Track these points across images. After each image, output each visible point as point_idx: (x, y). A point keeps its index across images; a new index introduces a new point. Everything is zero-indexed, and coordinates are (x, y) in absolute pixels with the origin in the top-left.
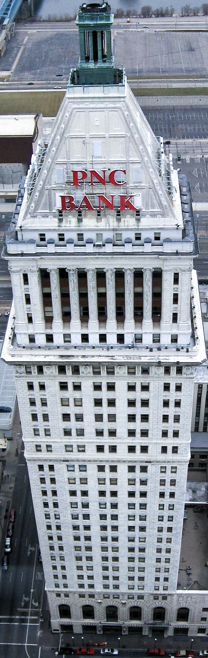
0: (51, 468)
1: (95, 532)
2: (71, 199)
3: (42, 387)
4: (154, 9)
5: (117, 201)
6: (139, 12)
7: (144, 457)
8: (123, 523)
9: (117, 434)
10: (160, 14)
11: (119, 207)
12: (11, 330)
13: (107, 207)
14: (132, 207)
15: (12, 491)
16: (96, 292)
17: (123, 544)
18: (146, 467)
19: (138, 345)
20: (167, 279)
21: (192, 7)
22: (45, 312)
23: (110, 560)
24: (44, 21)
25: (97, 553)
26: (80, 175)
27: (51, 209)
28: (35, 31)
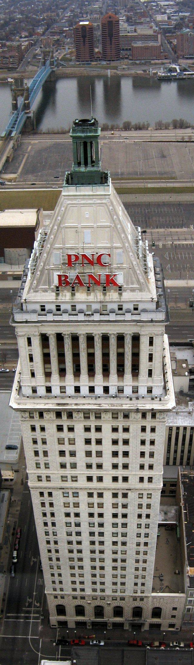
0: (50, 494)
3: (43, 429)
4: (133, 123)
5: (103, 279)
6: (121, 126)
7: (125, 485)
8: (108, 539)
9: (103, 467)
10: (138, 128)
14: (115, 284)
15: (18, 513)
16: (86, 352)
24: (44, 133)
26: (73, 258)
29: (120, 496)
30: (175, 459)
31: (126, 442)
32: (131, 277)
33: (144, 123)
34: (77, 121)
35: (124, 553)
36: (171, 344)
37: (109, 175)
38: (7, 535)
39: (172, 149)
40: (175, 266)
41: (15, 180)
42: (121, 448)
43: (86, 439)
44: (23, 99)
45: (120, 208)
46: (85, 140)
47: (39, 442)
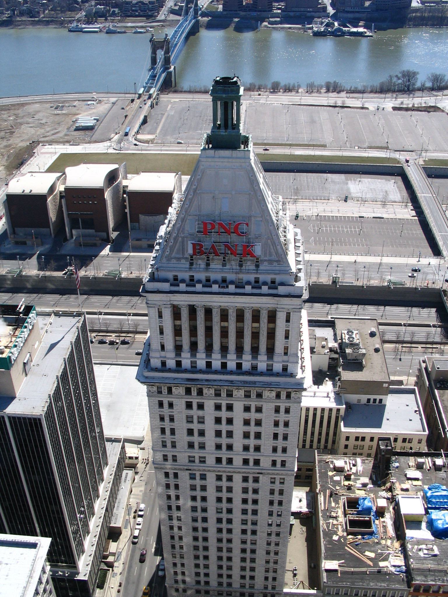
0: (176, 475)
1: (212, 534)
2: (201, 246)
3: (171, 405)
4: (282, 84)
5: (240, 249)
6: (270, 86)
7: (256, 469)
8: (237, 526)
9: (234, 448)
10: (288, 89)
11: (242, 254)
12: (146, 355)
13: (231, 254)
14: (252, 255)
15: (141, 493)
16: (219, 326)
17: (236, 546)
18: (258, 477)
19: (254, 372)
20: (281, 317)
21: (316, 84)
22: (176, 341)
23: (225, 559)
24: (185, 92)
25: (213, 553)
26: (209, 227)
27: (183, 253)
28: (177, 100)
29: (251, 480)
30: (312, 441)
31: (258, 423)
32: (270, 247)
33: (294, 84)
34: (218, 79)
35: (254, 543)
36: (310, 321)
37: (250, 139)
38: (127, 517)
39: (324, 114)
40: (319, 239)
41: (152, 141)
42: (253, 429)
43: (216, 418)
44: (163, 53)
45: (261, 175)
46: (226, 100)
47: (167, 419)
